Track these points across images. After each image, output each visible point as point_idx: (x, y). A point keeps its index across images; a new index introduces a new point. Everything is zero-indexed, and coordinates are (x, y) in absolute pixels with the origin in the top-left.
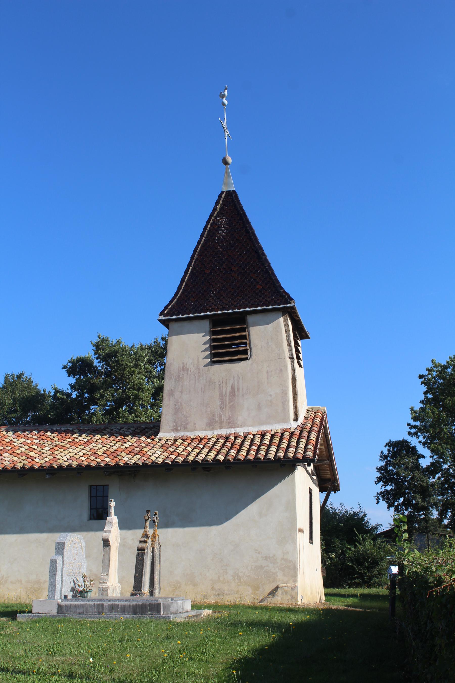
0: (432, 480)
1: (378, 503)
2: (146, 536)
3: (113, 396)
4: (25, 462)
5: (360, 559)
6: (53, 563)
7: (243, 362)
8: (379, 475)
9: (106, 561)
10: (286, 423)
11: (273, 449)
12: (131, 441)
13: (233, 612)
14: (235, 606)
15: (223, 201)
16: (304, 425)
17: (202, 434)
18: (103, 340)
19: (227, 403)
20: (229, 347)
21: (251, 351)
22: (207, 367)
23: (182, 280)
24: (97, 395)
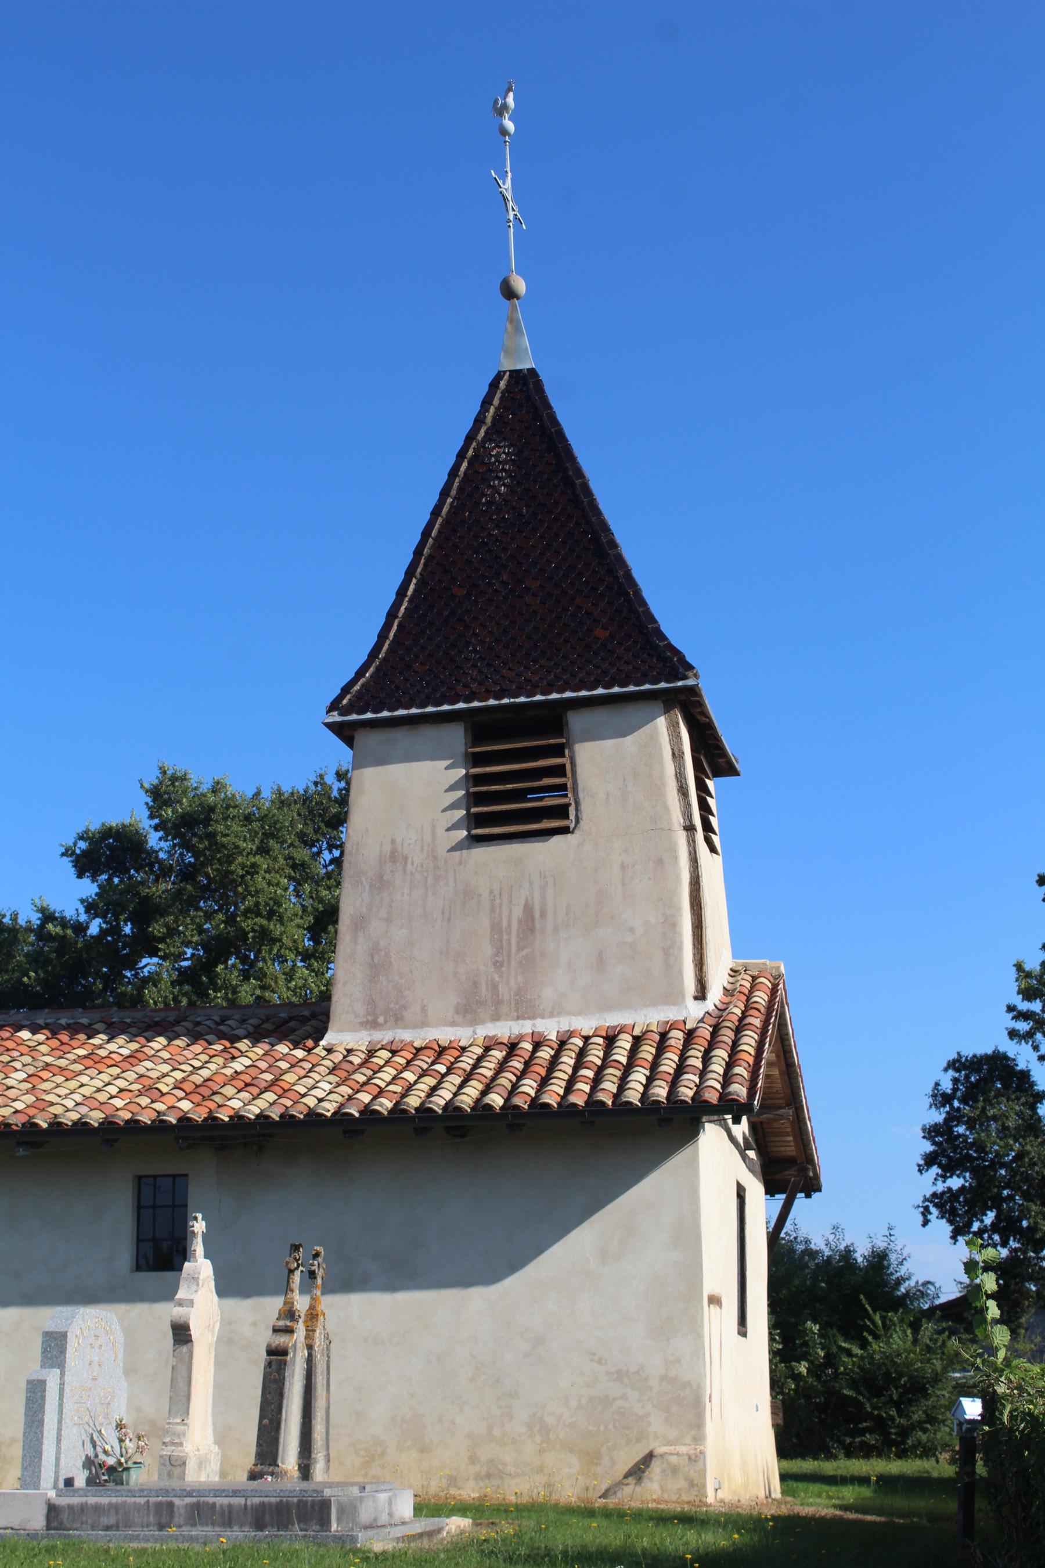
1: (926, 1223)
2: (290, 1314)
3: (200, 931)
5: (876, 1380)
6: (36, 1391)
7: (556, 839)
8: (928, 1147)
9: (181, 1384)
10: (674, 1004)
11: (639, 1076)
12: (250, 1055)
13: (529, 1523)
15: (501, 399)
16: (722, 1010)
17: (444, 1035)
18: (174, 779)
19: (514, 951)
20: (517, 795)
21: (577, 810)
22: (457, 853)
23: (391, 615)
24: (157, 929)
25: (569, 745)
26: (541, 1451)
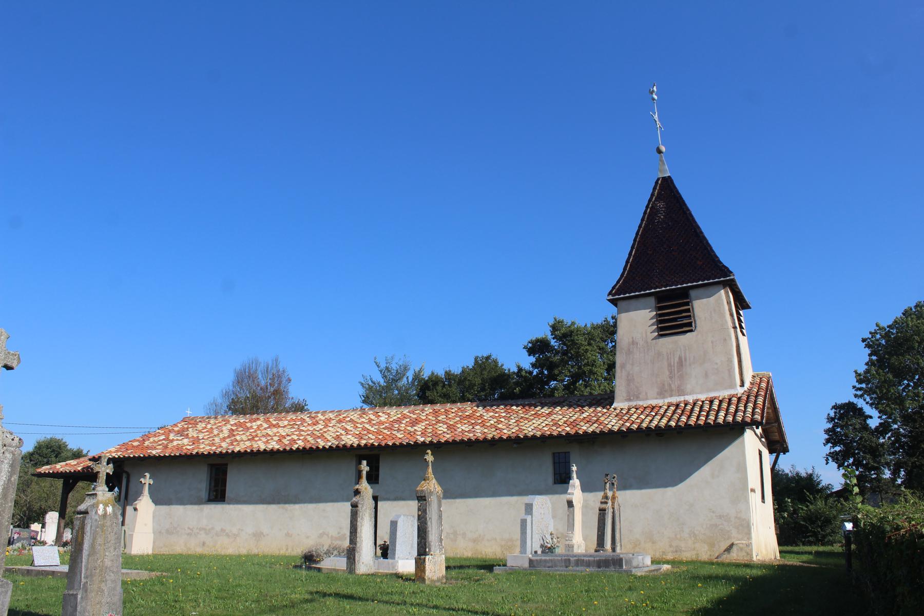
0: (882, 441)
3: (570, 371)
4: (495, 433)
5: (812, 518)
6: (524, 523)
7: (689, 334)
8: (827, 437)
11: (722, 414)
12: (588, 412)
13: (691, 567)
14: (692, 562)
16: (750, 390)
17: (654, 402)
20: (674, 320)
23: (627, 262)
24: (556, 372)
25: (691, 302)
26: (694, 543)
